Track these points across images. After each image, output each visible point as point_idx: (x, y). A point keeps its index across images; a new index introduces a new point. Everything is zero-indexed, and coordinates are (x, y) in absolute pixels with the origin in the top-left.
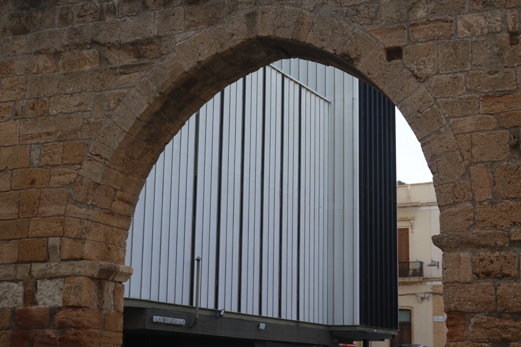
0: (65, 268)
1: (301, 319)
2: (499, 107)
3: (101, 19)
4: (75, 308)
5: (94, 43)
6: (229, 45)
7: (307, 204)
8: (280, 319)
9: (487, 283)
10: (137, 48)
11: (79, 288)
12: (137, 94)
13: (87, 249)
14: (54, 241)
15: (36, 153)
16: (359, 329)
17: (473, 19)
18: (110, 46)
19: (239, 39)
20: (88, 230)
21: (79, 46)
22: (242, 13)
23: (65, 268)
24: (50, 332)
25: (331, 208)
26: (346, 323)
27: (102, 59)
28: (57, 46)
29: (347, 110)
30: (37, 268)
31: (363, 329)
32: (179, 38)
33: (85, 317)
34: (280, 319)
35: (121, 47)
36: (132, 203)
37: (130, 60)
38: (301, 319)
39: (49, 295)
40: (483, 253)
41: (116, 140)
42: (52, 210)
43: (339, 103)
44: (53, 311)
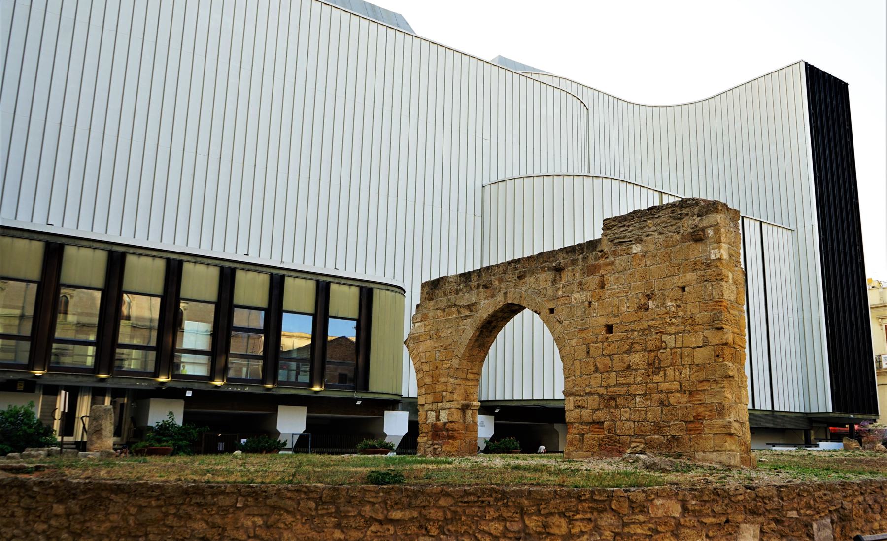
0: (448, 405)
1: (776, 409)
2: (584, 335)
3: (457, 294)
4: (451, 422)
5: (455, 305)
6: (498, 307)
7: (776, 316)
8: (773, 411)
9: (578, 410)
10: (470, 307)
11: (452, 414)
12: (469, 328)
13: (455, 397)
14: (444, 393)
15: (437, 355)
16: (831, 415)
17: (576, 295)
18: (461, 307)
19: (501, 304)
20: (455, 389)
21: (450, 306)
22: (502, 293)
23: (448, 405)
24: (444, 433)
25: (801, 317)
26: (820, 411)
27: (459, 312)
28: (443, 307)
29: (808, 235)
30: (440, 405)
31: (837, 415)
32: (482, 303)
33: (456, 426)
34: (773, 411)
35: (464, 307)
36: (479, 374)
37: (467, 313)
38: (776, 409)
39: (444, 417)
40: (577, 398)
41: (463, 349)
42: (443, 380)
43: (801, 230)
44: (445, 424)
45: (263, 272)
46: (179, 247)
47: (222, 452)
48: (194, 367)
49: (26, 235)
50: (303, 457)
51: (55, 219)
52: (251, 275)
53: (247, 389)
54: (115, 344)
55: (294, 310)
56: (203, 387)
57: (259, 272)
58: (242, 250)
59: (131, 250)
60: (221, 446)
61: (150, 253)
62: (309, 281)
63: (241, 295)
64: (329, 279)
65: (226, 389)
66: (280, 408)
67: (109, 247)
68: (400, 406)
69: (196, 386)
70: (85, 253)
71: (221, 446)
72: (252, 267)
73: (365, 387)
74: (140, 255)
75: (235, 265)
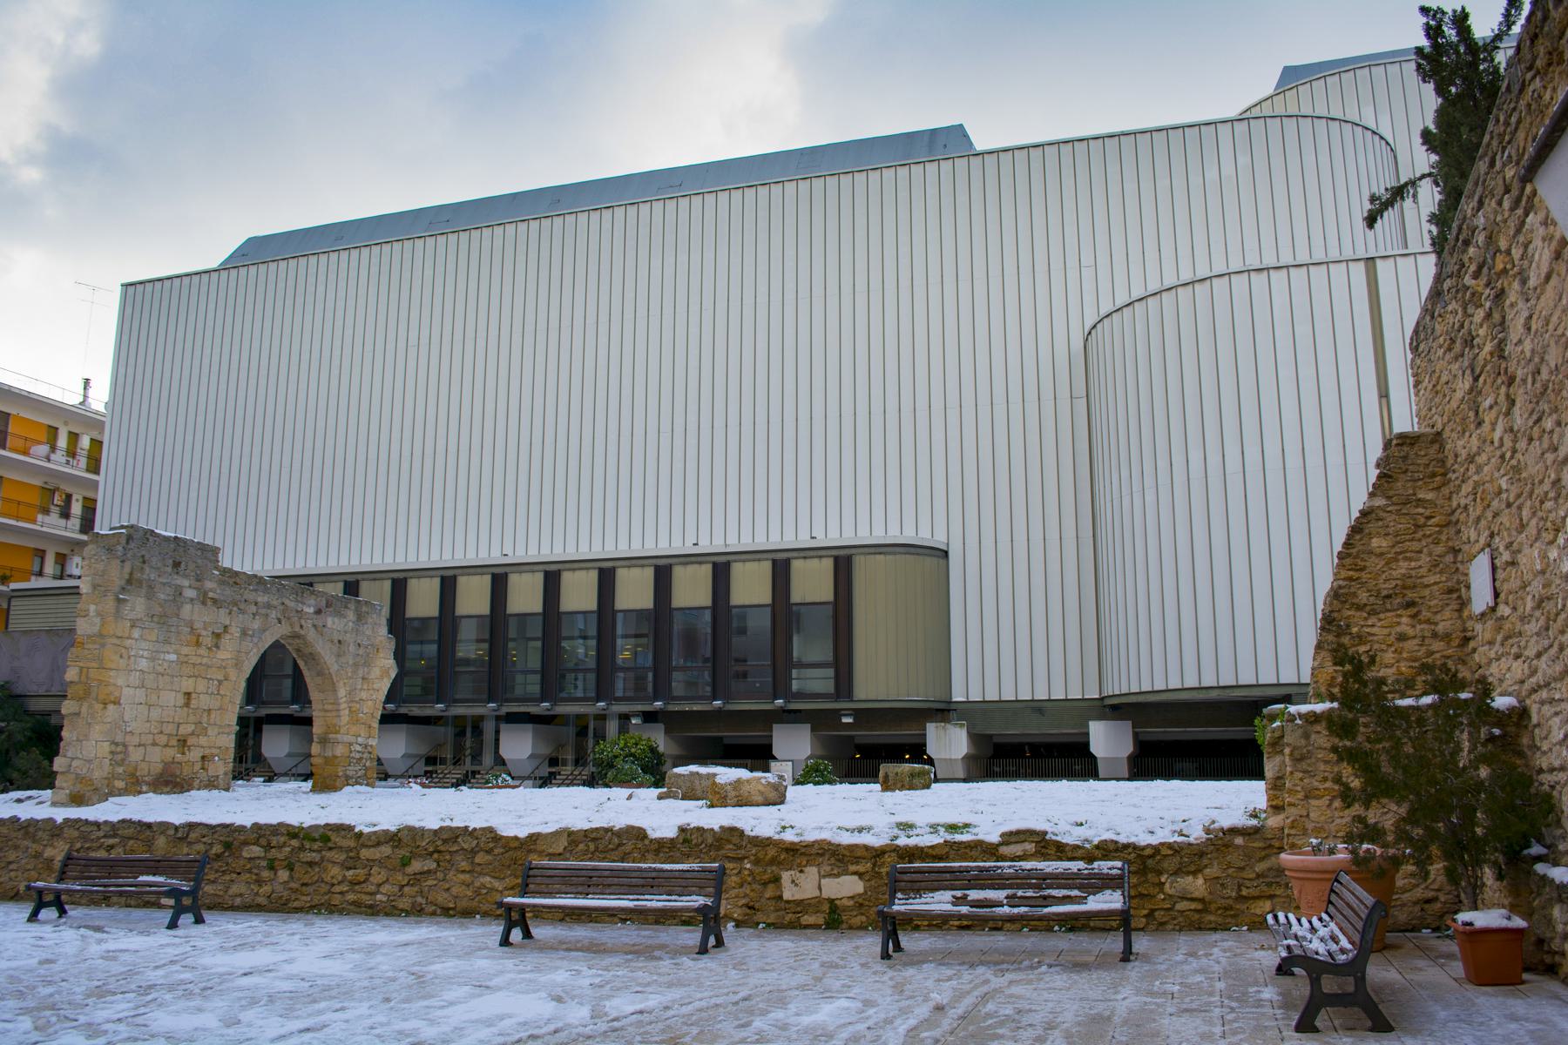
46: (848, 538)
54: (790, 664)
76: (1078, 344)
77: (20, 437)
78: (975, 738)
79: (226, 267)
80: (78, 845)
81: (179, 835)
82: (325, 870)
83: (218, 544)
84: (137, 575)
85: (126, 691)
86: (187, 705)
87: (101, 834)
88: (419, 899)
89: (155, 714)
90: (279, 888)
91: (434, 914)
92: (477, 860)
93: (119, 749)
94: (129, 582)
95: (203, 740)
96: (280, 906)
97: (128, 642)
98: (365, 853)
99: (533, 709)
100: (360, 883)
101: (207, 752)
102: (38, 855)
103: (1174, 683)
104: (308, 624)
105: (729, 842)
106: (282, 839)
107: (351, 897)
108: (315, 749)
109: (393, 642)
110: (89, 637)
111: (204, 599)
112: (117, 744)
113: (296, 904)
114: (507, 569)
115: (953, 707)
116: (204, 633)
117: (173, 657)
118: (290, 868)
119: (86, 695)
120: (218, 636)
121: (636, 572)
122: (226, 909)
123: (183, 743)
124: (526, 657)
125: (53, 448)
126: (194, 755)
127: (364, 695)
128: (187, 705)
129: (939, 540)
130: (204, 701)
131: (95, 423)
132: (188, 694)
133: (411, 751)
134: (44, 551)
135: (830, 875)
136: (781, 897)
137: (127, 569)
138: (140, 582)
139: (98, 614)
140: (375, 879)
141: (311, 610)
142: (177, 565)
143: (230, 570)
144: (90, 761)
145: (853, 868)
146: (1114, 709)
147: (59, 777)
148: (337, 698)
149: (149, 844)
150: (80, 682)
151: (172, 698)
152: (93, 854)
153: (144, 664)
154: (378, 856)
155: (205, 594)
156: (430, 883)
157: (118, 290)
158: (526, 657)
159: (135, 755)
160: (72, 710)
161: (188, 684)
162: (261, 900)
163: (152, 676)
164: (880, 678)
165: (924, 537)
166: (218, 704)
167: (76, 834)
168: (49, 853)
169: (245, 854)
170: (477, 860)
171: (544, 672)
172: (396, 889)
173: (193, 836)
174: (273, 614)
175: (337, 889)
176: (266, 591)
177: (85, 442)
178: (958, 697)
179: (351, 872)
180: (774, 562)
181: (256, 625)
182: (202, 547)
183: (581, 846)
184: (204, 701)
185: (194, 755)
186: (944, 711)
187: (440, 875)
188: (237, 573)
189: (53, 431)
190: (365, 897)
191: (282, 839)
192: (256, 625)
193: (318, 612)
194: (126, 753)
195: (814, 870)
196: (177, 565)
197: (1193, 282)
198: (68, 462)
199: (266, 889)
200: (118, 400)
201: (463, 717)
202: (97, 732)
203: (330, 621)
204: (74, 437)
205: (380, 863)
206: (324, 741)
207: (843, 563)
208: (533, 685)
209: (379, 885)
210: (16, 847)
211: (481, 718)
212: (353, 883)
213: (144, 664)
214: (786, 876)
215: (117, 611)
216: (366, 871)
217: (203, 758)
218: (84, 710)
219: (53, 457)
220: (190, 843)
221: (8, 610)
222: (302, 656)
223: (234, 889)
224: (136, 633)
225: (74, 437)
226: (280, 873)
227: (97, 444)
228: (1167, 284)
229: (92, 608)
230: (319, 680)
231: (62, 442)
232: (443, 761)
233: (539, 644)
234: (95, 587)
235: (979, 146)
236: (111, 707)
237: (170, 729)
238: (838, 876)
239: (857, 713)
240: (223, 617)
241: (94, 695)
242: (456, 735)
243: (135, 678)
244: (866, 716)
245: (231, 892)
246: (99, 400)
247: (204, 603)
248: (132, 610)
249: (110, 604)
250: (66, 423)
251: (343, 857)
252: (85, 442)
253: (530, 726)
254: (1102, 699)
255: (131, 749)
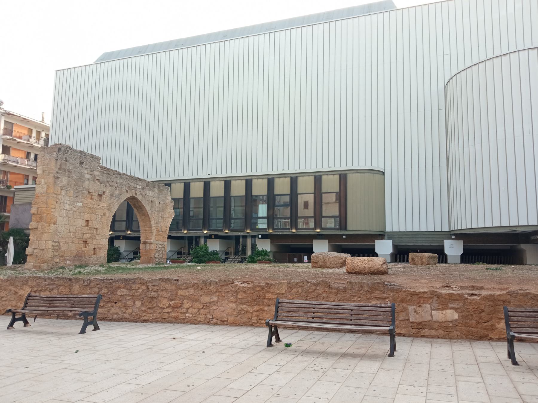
45: (287, 177)
46: (344, 168)
47: (296, 262)
48: (330, 224)
49: (199, 180)
50: (111, 265)
51: (286, 168)
52: (282, 179)
53: (284, 233)
54: (321, 217)
55: (304, 192)
56: (264, 233)
57: (285, 177)
58: (280, 168)
59: (233, 178)
60: (296, 260)
61: (240, 178)
62: (311, 177)
63: (278, 190)
64: (273, 176)
65: (274, 233)
66: (314, 241)
67: (184, 181)
68: (386, 237)
69: (262, 233)
70: (217, 183)
71: (296, 260)
72: (283, 176)
73: (346, 229)
74: (236, 180)
75: (190, 181)
76: (441, 86)
77: (17, 132)
78: (395, 247)
79: (96, 64)
80: (36, 289)
81: (86, 284)
82: (160, 301)
83: (101, 156)
84: (63, 167)
85: (59, 218)
86: (87, 225)
87: (47, 283)
88: (209, 316)
89: (73, 229)
90: (136, 310)
91: (216, 324)
92: (238, 296)
93: (57, 244)
94: (59, 169)
95: (94, 241)
96: (136, 319)
97: (60, 197)
98: (180, 292)
99: (220, 234)
100: (177, 308)
101: (96, 247)
102: (16, 293)
103: (488, 225)
104: (139, 193)
105: (377, 289)
106: (138, 286)
107: (173, 314)
108: (141, 246)
109: (173, 203)
110: (42, 194)
111: (95, 179)
112: (55, 242)
113: (145, 318)
114: (210, 180)
115: (386, 234)
116: (94, 194)
117: (80, 204)
118: (142, 300)
119: (40, 220)
120: (100, 196)
121: (260, 181)
122: (110, 320)
123: (85, 242)
124: (218, 213)
125: (31, 137)
126: (90, 247)
127: (162, 224)
128: (87, 225)
129: (381, 168)
130: (95, 224)
131: (46, 129)
132: (87, 221)
133: (174, 250)
134: (28, 176)
135: (437, 309)
136: (408, 320)
137: (59, 163)
138: (65, 170)
139: (46, 183)
140: (186, 306)
141: (140, 187)
142: (81, 163)
143: (105, 168)
144: (42, 250)
145: (451, 306)
146: (459, 236)
147: (28, 257)
148: (151, 224)
149: (70, 287)
150: (37, 214)
151: (81, 223)
152: (42, 294)
153: (67, 207)
154: (187, 294)
155: (94, 177)
156: (214, 308)
157: (54, 74)
158: (218, 213)
159: (64, 247)
160: (34, 227)
161: (87, 217)
162: (126, 316)
163: (71, 212)
164: (357, 224)
165: (374, 167)
166: (101, 226)
167: (35, 283)
168: (21, 292)
169: (119, 293)
170: (238, 296)
171: (225, 219)
172: (196, 311)
173: (92, 284)
174: (124, 188)
175: (166, 310)
176: (121, 178)
177: (43, 135)
178: (388, 229)
179: (173, 302)
180: (315, 177)
181: (117, 192)
182: (93, 157)
183: (294, 290)
184: (95, 224)
185: (90, 247)
186: (382, 236)
187: (219, 304)
188: (108, 169)
189: (31, 130)
190: (180, 315)
191: (138, 286)
192: (117, 192)
193: (143, 188)
194: (59, 246)
195: (428, 306)
196: (81, 163)
197: (501, 56)
198: (37, 142)
199: (130, 310)
200: (55, 119)
201: (192, 237)
202: (45, 236)
203: (148, 192)
204: (39, 133)
205: (189, 298)
206: (145, 243)
207: (343, 177)
208: (220, 225)
209: (188, 309)
210: (5, 290)
211: (198, 237)
212: (174, 308)
213: (67, 207)
214: (411, 308)
215: (55, 182)
216: (180, 302)
217: (94, 249)
218: (40, 226)
219: (30, 140)
220: (91, 288)
221: (14, 198)
222: (136, 207)
223: (113, 310)
224: (63, 193)
225: (39, 133)
226: (137, 303)
227: (47, 136)
228: (481, 60)
229: (43, 181)
230: (143, 217)
231: (34, 134)
232: (184, 253)
233: (223, 209)
234: (44, 171)
235: (398, 8)
236: (52, 225)
237: (79, 236)
238: (443, 309)
239: (346, 235)
240: (102, 188)
241: (44, 220)
242: (189, 243)
243: (63, 213)
244: (351, 237)
245: (111, 312)
246: (48, 122)
247: (94, 181)
248: (62, 182)
249: (51, 179)
250: (35, 127)
251: (169, 294)
252: (43, 135)
253: (218, 240)
254: (450, 231)
255: (61, 244)
